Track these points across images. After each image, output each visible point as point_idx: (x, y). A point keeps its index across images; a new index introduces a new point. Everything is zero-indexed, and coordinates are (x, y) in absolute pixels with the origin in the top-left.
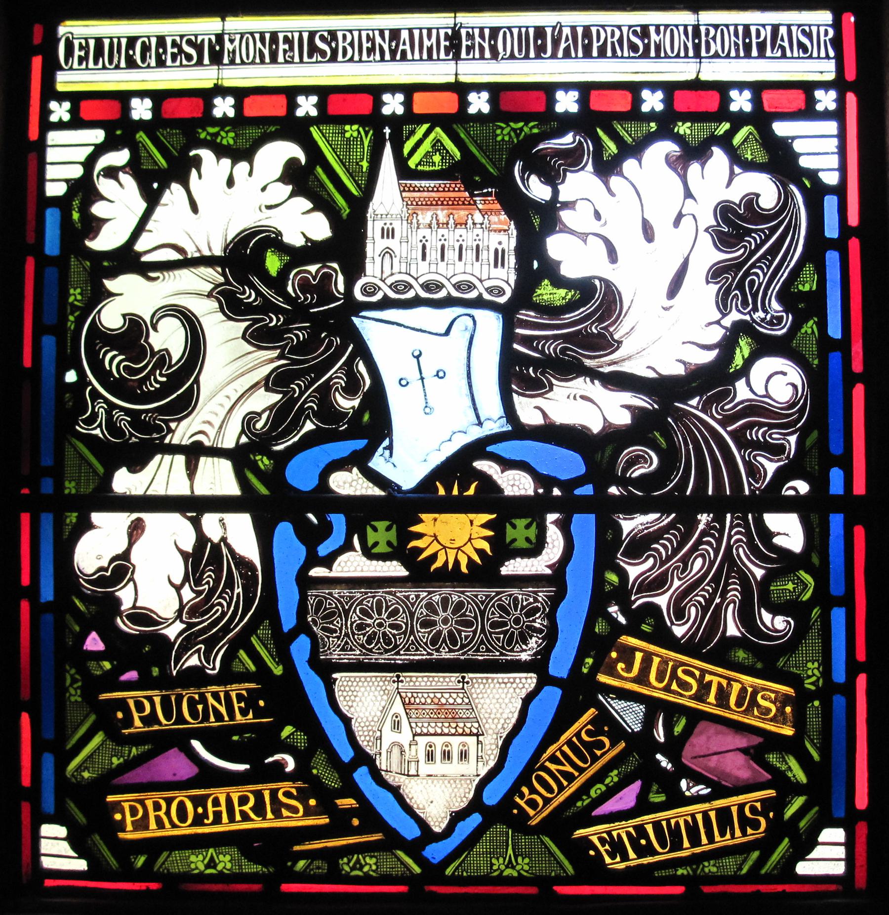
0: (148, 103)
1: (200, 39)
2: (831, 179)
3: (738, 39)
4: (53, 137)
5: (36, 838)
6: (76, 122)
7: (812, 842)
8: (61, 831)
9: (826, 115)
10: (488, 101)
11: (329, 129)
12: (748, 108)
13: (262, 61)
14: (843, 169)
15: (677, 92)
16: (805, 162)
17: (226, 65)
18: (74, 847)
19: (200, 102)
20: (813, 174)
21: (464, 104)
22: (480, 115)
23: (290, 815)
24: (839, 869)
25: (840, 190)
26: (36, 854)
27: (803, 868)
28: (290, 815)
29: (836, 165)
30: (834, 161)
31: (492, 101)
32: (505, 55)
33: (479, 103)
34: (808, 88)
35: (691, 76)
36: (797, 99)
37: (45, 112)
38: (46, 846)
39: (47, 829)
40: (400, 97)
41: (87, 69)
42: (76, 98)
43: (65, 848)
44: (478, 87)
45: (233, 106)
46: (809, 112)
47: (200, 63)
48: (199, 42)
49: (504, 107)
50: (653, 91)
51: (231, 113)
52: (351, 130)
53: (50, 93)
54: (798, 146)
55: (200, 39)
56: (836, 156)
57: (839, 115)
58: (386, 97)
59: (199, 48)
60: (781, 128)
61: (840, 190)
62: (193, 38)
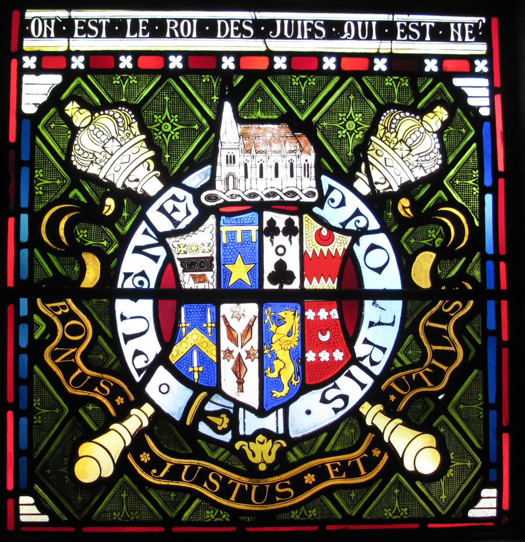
0: (435, 61)
1: (100, 21)
2: (485, 112)
3: (51, 27)
4: (26, 78)
5: (17, 505)
6: (39, 70)
7: (477, 498)
8: (30, 500)
9: (481, 75)
10: (223, 63)
11: (194, 78)
12: (333, 67)
13: (49, 36)
14: (492, 106)
15: (190, 57)
16: (471, 102)
17: (45, 38)
18: (39, 508)
19: (112, 58)
20: (475, 109)
21: (272, 63)
22: (280, 70)
23: (207, 487)
24: (493, 513)
25: (491, 118)
26: (17, 514)
27: (472, 513)
28: (207, 487)
29: (488, 104)
30: (486, 102)
31: (288, 63)
32: (349, 36)
33: (280, 63)
34: (471, 59)
35: (64, 49)
36: (464, 66)
37: (490, 65)
38: (23, 510)
39: (24, 499)
40: (334, 59)
41: (138, 37)
42: (40, 55)
43: (34, 510)
44: (280, 54)
45: (223, 63)
46: (471, 73)
47: (99, 36)
48: (100, 22)
49: (295, 67)
50: (176, 56)
51: (130, 66)
52: (206, 79)
53: (21, 53)
54: (468, 91)
55: (100, 21)
56: (488, 99)
57: (488, 75)
58: (122, 58)
59: (99, 26)
60: (457, 82)
61: (491, 118)
62: (96, 21)
